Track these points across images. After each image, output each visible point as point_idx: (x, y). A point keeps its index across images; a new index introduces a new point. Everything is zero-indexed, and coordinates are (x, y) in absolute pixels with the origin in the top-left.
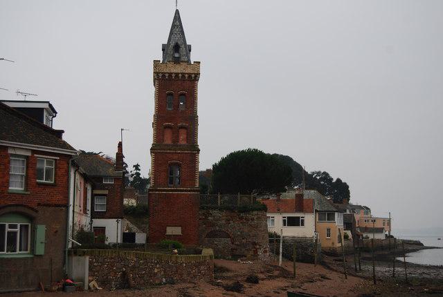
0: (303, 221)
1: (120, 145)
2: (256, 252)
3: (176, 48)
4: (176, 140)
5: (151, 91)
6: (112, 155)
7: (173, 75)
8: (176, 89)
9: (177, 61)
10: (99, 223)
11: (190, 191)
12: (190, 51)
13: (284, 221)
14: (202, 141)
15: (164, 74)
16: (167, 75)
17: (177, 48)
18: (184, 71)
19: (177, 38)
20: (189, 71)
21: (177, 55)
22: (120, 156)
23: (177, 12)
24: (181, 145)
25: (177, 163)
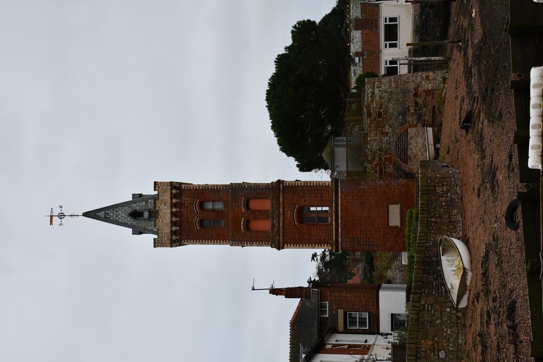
0: (391, 20)
1: (274, 291)
2: (428, 92)
3: (136, 214)
4: (263, 214)
5: (193, 252)
6: (293, 304)
7: (174, 219)
8: (193, 214)
9: (154, 214)
10: (385, 324)
11: (337, 194)
12: (141, 195)
13: (392, 46)
14: (269, 178)
15: (173, 233)
16: (174, 228)
17: (136, 215)
18: (168, 204)
19: (123, 215)
20: (167, 197)
21: (146, 215)
22: (290, 293)
23: (86, 214)
24: (273, 207)
25: (298, 212)
